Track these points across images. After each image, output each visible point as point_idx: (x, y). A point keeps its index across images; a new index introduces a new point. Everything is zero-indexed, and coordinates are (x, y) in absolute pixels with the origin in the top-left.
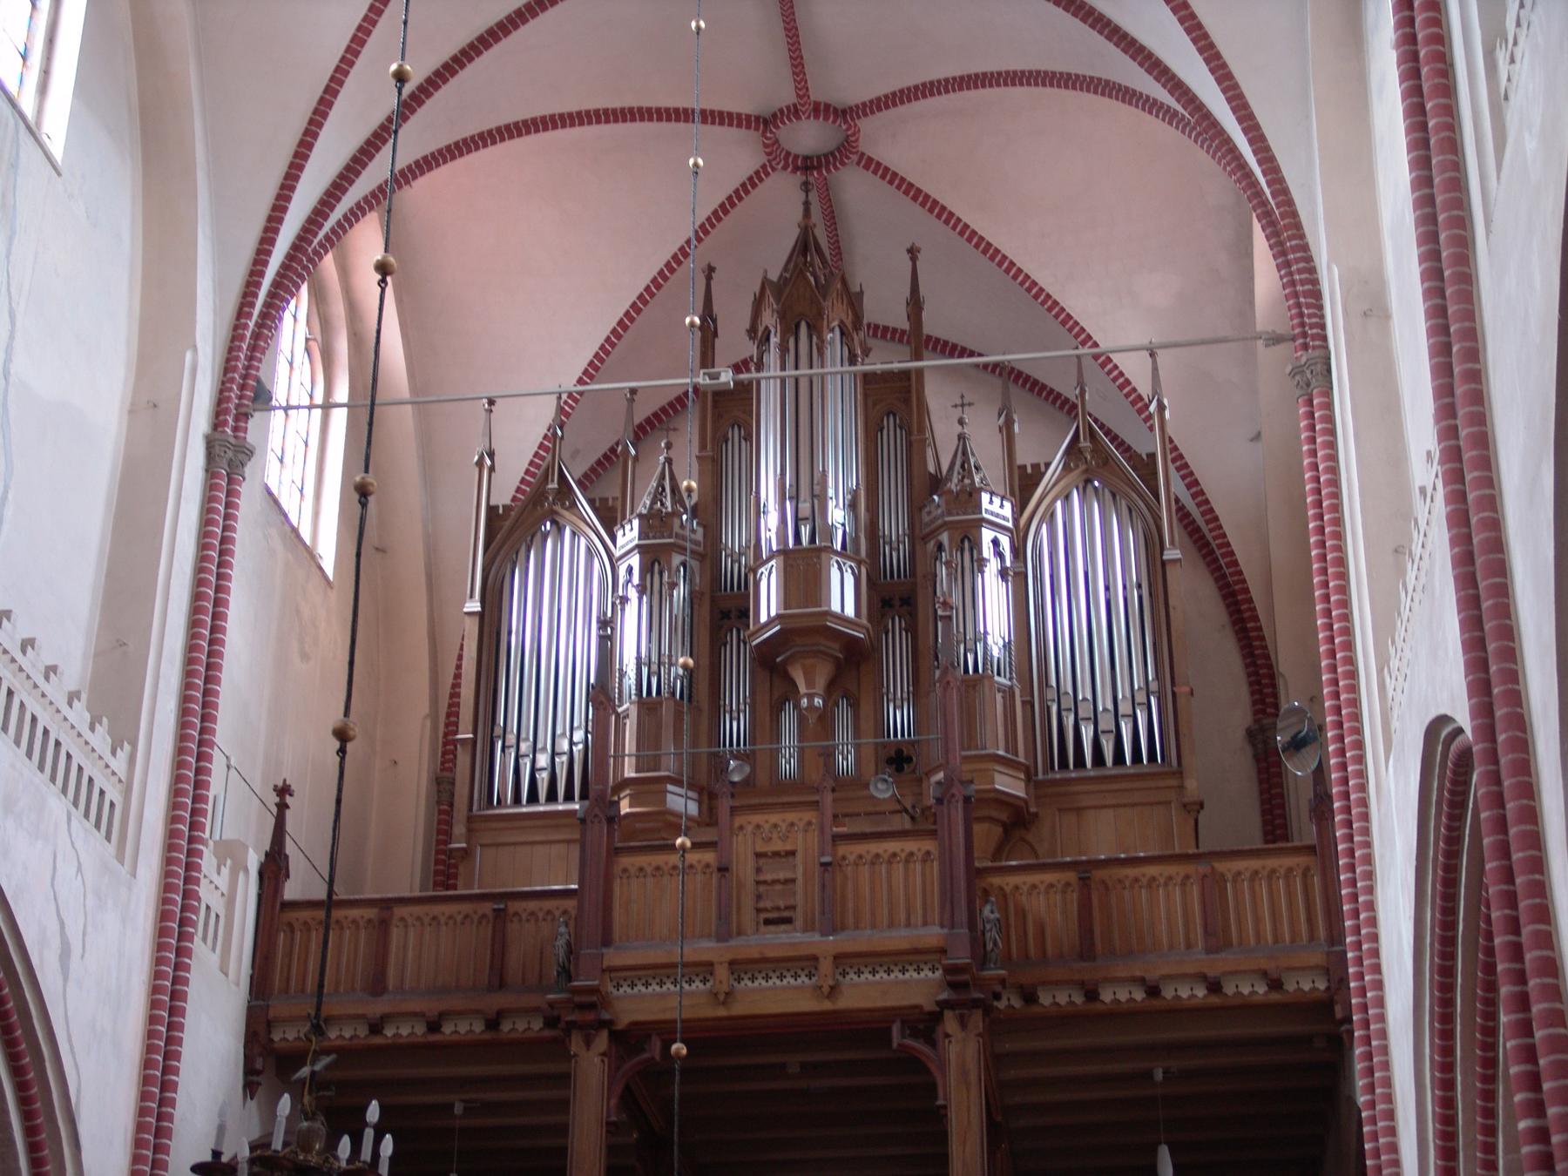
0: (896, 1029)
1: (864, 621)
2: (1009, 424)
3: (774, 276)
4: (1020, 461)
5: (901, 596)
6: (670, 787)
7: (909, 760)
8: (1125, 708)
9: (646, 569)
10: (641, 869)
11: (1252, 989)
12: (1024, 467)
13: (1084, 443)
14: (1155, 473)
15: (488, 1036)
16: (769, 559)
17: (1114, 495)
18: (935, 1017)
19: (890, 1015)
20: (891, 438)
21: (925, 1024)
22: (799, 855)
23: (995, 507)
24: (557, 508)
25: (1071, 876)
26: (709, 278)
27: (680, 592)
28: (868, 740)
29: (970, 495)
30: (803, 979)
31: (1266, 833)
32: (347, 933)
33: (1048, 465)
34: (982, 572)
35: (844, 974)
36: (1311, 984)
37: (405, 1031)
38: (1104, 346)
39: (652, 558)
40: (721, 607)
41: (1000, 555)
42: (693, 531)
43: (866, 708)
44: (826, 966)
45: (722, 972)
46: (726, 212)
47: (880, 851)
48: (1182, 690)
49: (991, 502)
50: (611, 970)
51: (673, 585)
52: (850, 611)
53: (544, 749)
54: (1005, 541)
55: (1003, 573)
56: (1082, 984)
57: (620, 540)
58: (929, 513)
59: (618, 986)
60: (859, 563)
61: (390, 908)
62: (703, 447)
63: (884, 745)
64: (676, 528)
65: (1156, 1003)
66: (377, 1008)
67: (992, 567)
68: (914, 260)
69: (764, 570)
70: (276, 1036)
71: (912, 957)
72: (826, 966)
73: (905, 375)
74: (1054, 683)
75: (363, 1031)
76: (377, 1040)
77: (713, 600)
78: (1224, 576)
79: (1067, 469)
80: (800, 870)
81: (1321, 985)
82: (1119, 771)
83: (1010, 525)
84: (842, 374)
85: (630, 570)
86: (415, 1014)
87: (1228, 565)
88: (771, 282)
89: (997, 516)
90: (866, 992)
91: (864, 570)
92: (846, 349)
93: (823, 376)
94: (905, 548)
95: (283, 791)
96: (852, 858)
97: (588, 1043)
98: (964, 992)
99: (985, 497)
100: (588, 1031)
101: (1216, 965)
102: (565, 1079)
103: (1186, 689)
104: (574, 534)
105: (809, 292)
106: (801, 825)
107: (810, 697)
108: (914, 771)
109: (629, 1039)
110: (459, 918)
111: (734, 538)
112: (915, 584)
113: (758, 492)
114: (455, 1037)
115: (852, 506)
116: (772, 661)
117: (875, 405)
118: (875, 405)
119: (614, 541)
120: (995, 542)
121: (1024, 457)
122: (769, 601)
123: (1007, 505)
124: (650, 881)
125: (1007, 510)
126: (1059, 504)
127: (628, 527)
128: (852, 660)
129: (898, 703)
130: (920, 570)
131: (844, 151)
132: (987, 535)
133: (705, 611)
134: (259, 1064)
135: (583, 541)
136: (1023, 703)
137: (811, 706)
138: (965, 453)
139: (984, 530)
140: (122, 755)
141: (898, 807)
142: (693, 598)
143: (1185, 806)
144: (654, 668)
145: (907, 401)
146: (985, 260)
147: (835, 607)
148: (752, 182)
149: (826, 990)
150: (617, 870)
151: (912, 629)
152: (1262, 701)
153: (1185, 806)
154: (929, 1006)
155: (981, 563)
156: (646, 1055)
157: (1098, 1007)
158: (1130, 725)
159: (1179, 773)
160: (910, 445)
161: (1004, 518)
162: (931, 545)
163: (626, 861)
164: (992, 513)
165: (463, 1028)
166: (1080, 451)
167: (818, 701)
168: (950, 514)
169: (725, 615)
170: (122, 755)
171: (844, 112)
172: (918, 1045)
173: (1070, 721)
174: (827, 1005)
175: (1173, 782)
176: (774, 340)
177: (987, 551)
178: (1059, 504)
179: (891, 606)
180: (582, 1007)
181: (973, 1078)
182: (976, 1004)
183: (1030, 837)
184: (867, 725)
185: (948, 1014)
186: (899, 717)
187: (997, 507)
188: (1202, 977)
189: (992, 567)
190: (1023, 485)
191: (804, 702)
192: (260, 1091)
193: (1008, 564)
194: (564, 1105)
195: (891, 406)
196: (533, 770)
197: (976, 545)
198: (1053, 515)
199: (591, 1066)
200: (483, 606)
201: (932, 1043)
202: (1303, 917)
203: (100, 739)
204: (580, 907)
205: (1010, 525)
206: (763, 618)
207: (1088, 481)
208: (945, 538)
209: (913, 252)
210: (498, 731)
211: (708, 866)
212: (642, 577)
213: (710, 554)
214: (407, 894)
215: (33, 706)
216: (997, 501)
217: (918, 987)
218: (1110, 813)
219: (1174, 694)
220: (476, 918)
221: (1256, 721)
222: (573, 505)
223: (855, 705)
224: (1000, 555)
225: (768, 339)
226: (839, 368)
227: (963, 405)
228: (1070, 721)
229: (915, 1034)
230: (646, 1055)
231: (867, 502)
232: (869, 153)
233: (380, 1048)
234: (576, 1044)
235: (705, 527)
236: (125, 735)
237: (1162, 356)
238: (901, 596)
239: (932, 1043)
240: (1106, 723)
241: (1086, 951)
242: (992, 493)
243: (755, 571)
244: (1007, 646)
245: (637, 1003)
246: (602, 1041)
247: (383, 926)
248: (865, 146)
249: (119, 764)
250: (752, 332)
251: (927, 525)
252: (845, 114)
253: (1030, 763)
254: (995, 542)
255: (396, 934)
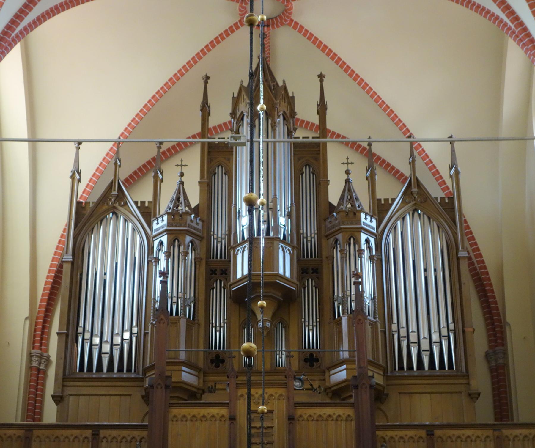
1: (295, 281)
3: (245, 84)
4: (378, 197)
5: (313, 267)
6: (184, 368)
7: (317, 360)
8: (435, 337)
9: (171, 244)
10: (184, 416)
12: (379, 200)
13: (414, 189)
14: (454, 208)
16: (241, 244)
17: (429, 219)
20: (307, 177)
23: (368, 222)
24: (116, 205)
25: (423, 433)
26: (206, 83)
27: (190, 256)
29: (355, 214)
33: (393, 200)
34: (361, 258)
39: (175, 236)
41: (370, 248)
42: (197, 224)
43: (293, 329)
47: (322, 414)
48: (468, 330)
49: (366, 218)
51: (186, 254)
52: (288, 274)
53: (97, 336)
54: (372, 241)
55: (371, 258)
57: (155, 226)
58: (330, 222)
60: (293, 248)
61: (31, 431)
64: (188, 222)
67: (366, 254)
68: (321, 81)
74: (395, 321)
77: (207, 263)
79: (404, 202)
80: (276, 421)
83: (375, 231)
84: (284, 142)
85: (161, 243)
88: (244, 87)
89: (369, 226)
91: (295, 252)
92: (286, 127)
93: (275, 142)
94: (315, 240)
96: (305, 417)
99: (363, 216)
103: (470, 330)
104: (125, 221)
105: (265, 91)
106: (277, 396)
107: (264, 321)
108: (319, 367)
110: (72, 438)
111: (219, 229)
112: (322, 261)
113: (236, 204)
115: (289, 215)
116: (242, 298)
117: (299, 160)
118: (299, 160)
119: (150, 225)
120: (367, 241)
121: (380, 195)
122: (241, 267)
123: (374, 221)
124: (189, 423)
125: (374, 224)
126: (399, 222)
127: (160, 219)
128: (286, 300)
129: (311, 327)
130: (325, 254)
135: (130, 224)
136: (381, 331)
137: (264, 327)
138: (349, 190)
139: (362, 234)
141: (310, 387)
142: (197, 261)
143: (470, 395)
144: (175, 300)
145: (317, 159)
146: (332, 63)
150: (171, 416)
151: (319, 287)
153: (470, 395)
155: (361, 252)
158: (438, 348)
159: (467, 376)
161: (373, 228)
163: (175, 411)
164: (366, 225)
166: (412, 193)
167: (268, 324)
168: (344, 224)
169: (214, 272)
173: (404, 344)
175: (464, 381)
176: (246, 120)
177: (363, 246)
178: (399, 222)
179: (307, 273)
183: (382, 407)
184: (294, 340)
186: (311, 335)
187: (368, 221)
190: (380, 209)
191: (260, 324)
193: (374, 253)
195: (309, 159)
197: (357, 242)
198: (395, 228)
200: (73, 258)
202: (69, 344)
205: (375, 231)
206: (239, 275)
207: (415, 210)
208: (340, 237)
209: (321, 77)
210: (80, 330)
211: (223, 416)
212: (169, 248)
213: (203, 237)
216: (369, 218)
218: (428, 396)
219: (464, 332)
220: (81, 439)
222: (126, 204)
223: (286, 327)
224: (370, 248)
225: (242, 119)
226: (282, 139)
227: (348, 163)
228: (404, 344)
231: (295, 215)
235: (203, 221)
238: (313, 267)
240: (425, 345)
242: (366, 214)
250: (233, 114)
253: (384, 365)
254: (367, 241)
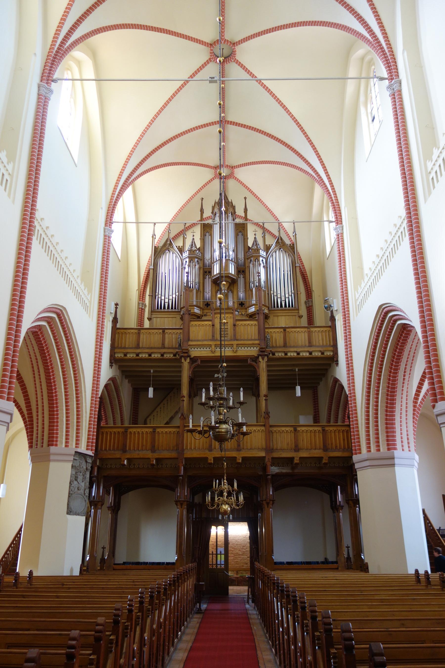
0: (249, 360)
1: (236, 275)
2: (264, 236)
3: (217, 201)
4: (266, 244)
5: (242, 270)
7: (244, 304)
8: (287, 296)
9: (190, 262)
11: (318, 354)
12: (267, 245)
15: (161, 358)
18: (257, 357)
19: (248, 357)
20: (240, 237)
21: (255, 359)
22: (229, 323)
23: (263, 253)
24: (169, 247)
25: (282, 330)
26: (202, 201)
28: (236, 300)
30: (208, 349)
31: (308, 323)
32: (127, 335)
33: (272, 245)
35: (238, 348)
36: (329, 354)
37: (131, 356)
38: (281, 221)
39: (191, 259)
40: (206, 271)
43: (235, 293)
44: (235, 346)
45: (213, 347)
46: (205, 187)
48: (299, 293)
50: (190, 345)
52: (233, 273)
54: (264, 260)
55: (264, 267)
56: (284, 352)
57: (184, 255)
59: (191, 349)
60: (235, 263)
62: (201, 237)
63: (204, 302)
65: (299, 356)
66: (138, 351)
67: (262, 265)
69: (215, 263)
70: (116, 356)
71: (253, 345)
72: (235, 346)
73: (244, 224)
75: (135, 356)
76: (138, 357)
78: (302, 271)
79: (276, 245)
81: (332, 354)
82: (286, 308)
85: (186, 262)
86: (146, 352)
87: (303, 268)
90: (243, 352)
93: (228, 223)
95: (117, 305)
97: (185, 360)
98: (262, 352)
99: (261, 251)
100: (185, 358)
101: (311, 349)
102: (180, 367)
107: (224, 290)
109: (193, 360)
111: (208, 256)
114: (315, 356)
115: (234, 251)
116: (216, 282)
120: (262, 260)
121: (267, 243)
122: (216, 270)
123: (265, 253)
125: (265, 254)
126: (274, 253)
128: (232, 282)
130: (247, 265)
131: (231, 176)
132: (261, 259)
133: (202, 271)
134: (113, 362)
140: (90, 295)
142: (200, 268)
147: (231, 272)
148: (210, 181)
149: (235, 351)
150: (191, 325)
151: (245, 277)
152: (309, 297)
154: (256, 356)
155: (260, 264)
156: (197, 363)
157: (287, 356)
159: (298, 310)
160: (244, 239)
162: (249, 260)
165: (156, 356)
167: (226, 291)
170: (90, 295)
171: (232, 167)
172: (254, 363)
174: (235, 354)
177: (261, 262)
178: (274, 253)
180: (184, 353)
181: (265, 370)
182: (266, 355)
183: (267, 321)
184: (235, 297)
185: (260, 357)
186: (242, 295)
188: (308, 351)
189: (262, 265)
190: (267, 248)
192: (113, 367)
194: (180, 372)
196: (164, 302)
197: (259, 261)
199: (186, 364)
201: (256, 363)
203: (86, 292)
204: (183, 332)
206: (215, 274)
207: (280, 249)
208: (252, 259)
209: (245, 198)
210: (157, 294)
212: (189, 263)
213: (202, 259)
214: (133, 327)
215: (75, 285)
217: (253, 351)
221: (307, 299)
222: (173, 247)
224: (263, 263)
229: (253, 361)
230: (197, 363)
232: (235, 176)
233: (150, 359)
234: (183, 360)
236: (90, 291)
237: (296, 223)
238: (242, 270)
239: (256, 363)
241: (285, 345)
243: (213, 263)
244: (264, 282)
245: (195, 352)
246: (188, 360)
247: (139, 333)
248: (236, 175)
249: (89, 297)
250: (212, 213)
251: (248, 256)
252: (233, 167)
254: (262, 260)
255: (141, 336)
